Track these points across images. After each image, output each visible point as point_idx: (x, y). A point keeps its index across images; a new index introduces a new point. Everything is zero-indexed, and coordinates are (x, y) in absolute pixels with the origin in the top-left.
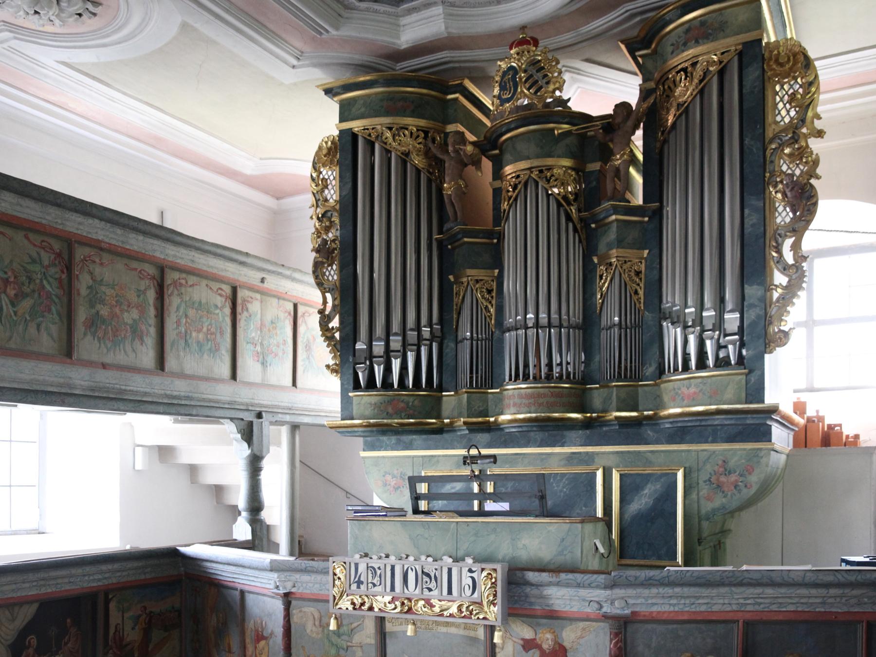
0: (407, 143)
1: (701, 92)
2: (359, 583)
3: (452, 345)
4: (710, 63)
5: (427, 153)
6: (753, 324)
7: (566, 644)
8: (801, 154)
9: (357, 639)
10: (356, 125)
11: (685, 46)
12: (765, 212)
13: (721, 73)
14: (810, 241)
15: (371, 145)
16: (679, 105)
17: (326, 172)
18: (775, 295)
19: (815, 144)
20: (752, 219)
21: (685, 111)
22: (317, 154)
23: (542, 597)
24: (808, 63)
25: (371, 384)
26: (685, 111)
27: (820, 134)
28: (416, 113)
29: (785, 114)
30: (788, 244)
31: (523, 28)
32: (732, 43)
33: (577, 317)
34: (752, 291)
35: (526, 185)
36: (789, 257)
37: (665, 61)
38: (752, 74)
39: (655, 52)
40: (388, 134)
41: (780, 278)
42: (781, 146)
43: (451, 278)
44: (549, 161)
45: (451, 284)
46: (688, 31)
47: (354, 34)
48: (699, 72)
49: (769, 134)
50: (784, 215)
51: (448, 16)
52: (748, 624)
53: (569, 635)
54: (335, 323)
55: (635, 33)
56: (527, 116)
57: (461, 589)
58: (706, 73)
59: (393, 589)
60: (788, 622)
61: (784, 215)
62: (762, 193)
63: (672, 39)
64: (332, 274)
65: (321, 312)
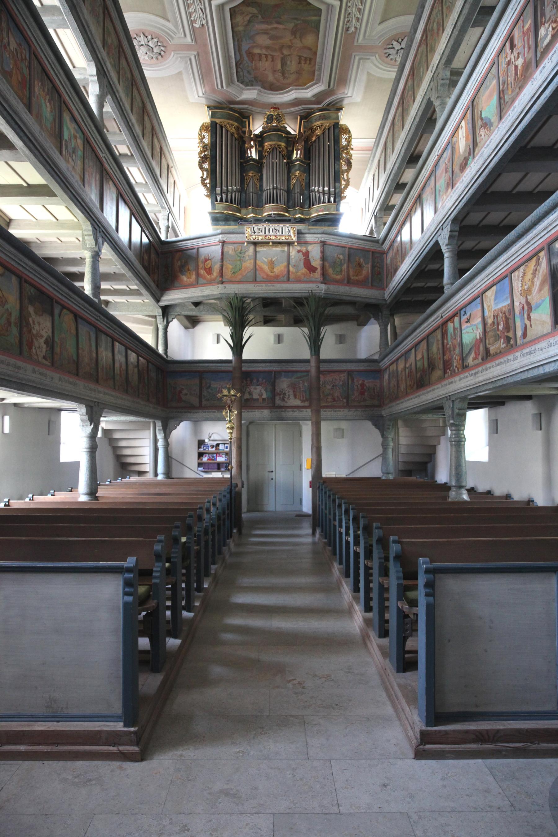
0: (233, 130)
1: (323, 133)
2: (255, 232)
3: (244, 195)
4: (326, 126)
5: (238, 134)
6: (338, 192)
7: (309, 250)
8: (348, 153)
9: (247, 254)
10: (218, 121)
11: (319, 120)
12: (340, 165)
13: (329, 129)
14: (351, 174)
15: (222, 127)
16: (317, 135)
17: (204, 133)
18: (342, 187)
19: (351, 152)
20: (337, 167)
21: (318, 137)
22: (201, 127)
23: (304, 237)
24: (349, 132)
25: (221, 200)
26: (318, 137)
27: (352, 149)
28: (236, 121)
29: (344, 143)
30: (345, 174)
31: (275, 104)
32: (332, 122)
33: (286, 188)
34: (337, 184)
35: (273, 149)
36: (346, 178)
37: (312, 123)
38: (337, 131)
39: (308, 121)
40: (228, 125)
41: (343, 183)
42: (344, 151)
43: (244, 174)
44: (280, 143)
45: (244, 177)
46: (320, 116)
47: (230, 91)
48: (323, 128)
49: (341, 147)
50: (344, 167)
51: (258, 94)
52: (349, 248)
53: (310, 248)
54: (207, 181)
55: (303, 114)
56: (276, 129)
57: (285, 232)
58: (325, 128)
59: (265, 233)
60: (357, 249)
61: (344, 167)
62: (339, 161)
63: (315, 118)
64: (206, 166)
65: (202, 177)
